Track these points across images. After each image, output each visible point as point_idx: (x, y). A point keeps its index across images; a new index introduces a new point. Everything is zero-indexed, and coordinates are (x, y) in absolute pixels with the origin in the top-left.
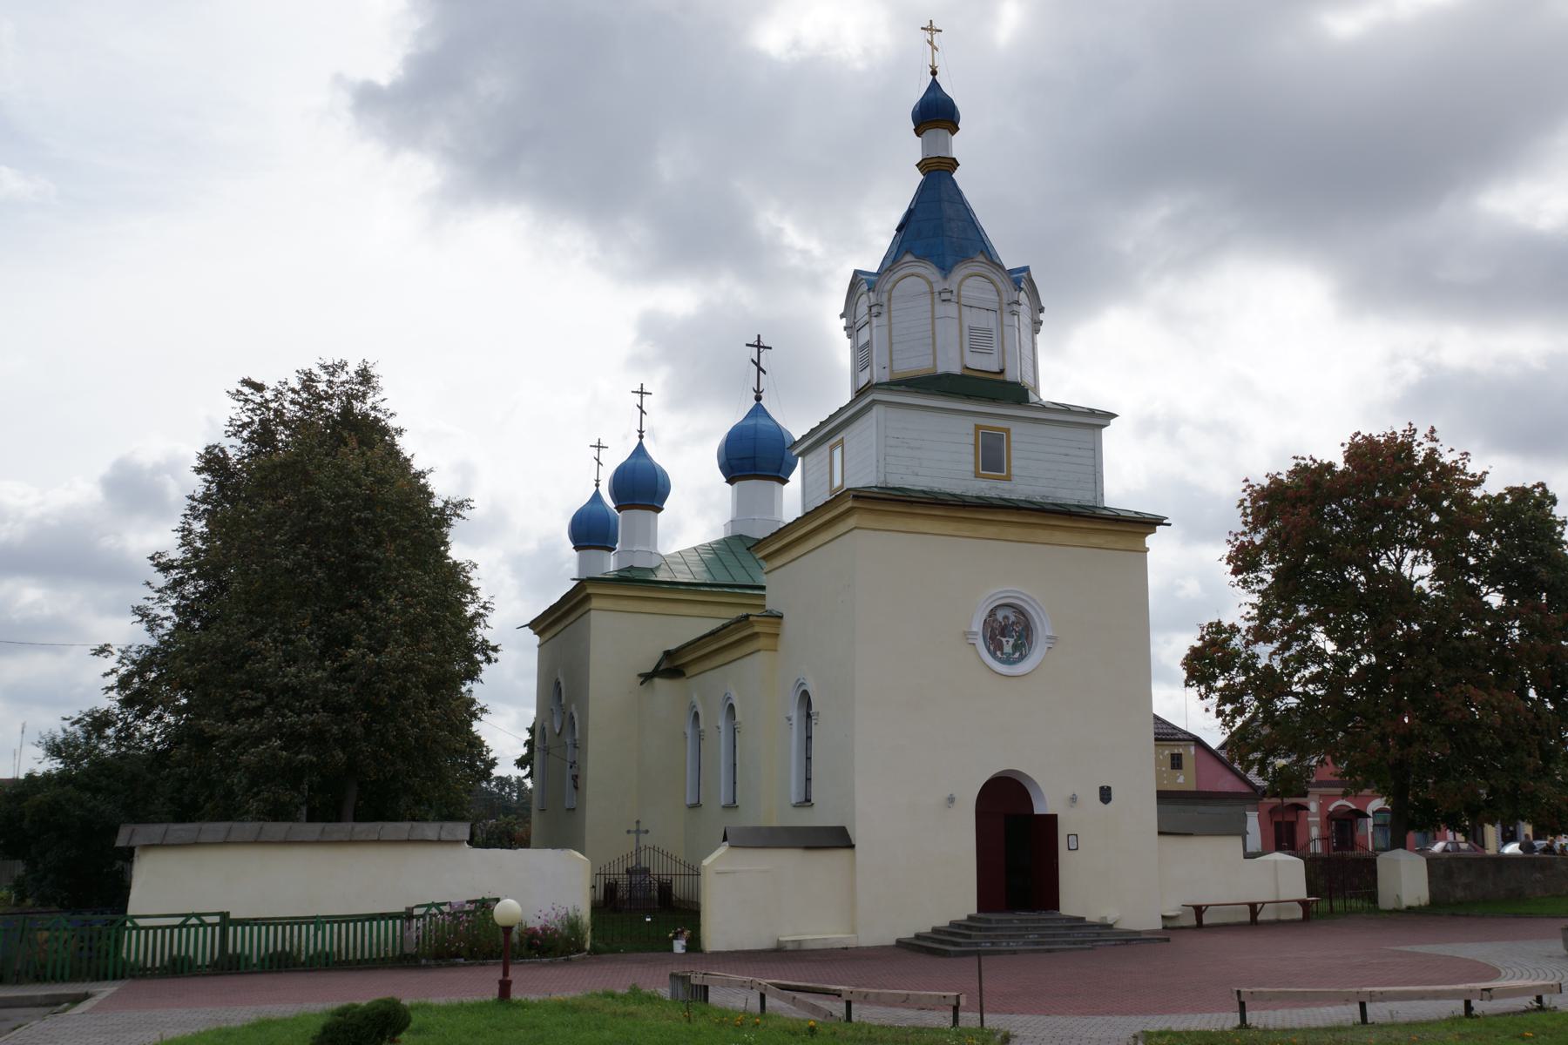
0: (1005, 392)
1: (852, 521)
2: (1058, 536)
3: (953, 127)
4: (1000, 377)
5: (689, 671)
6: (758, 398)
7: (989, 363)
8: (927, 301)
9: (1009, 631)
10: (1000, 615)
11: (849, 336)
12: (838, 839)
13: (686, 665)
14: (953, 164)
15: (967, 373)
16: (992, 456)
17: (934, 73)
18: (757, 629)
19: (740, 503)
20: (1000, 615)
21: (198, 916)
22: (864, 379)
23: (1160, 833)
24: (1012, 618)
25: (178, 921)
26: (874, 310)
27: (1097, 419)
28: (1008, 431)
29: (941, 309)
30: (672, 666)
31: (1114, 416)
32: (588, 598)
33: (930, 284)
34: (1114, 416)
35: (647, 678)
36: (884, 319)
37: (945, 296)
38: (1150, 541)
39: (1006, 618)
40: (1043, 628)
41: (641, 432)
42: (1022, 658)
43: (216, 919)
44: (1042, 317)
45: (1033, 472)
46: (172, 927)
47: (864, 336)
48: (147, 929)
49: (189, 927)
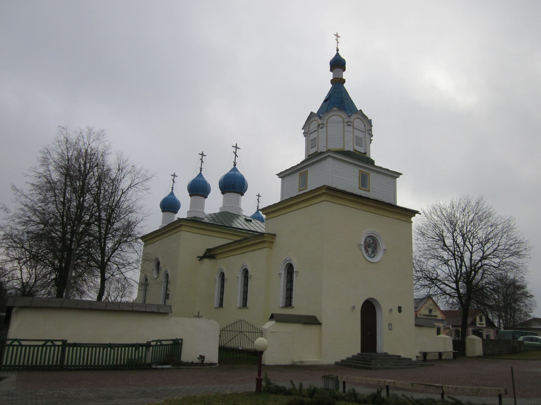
0: (363, 159)
1: (323, 198)
2: (386, 214)
3: (344, 70)
4: (364, 155)
5: (218, 257)
6: (235, 165)
7: (361, 150)
8: (341, 125)
9: (372, 245)
10: (368, 240)
11: (305, 136)
12: (312, 321)
13: (217, 254)
14: (344, 81)
15: (355, 152)
16: (364, 181)
17: (338, 50)
18: (266, 239)
19: (225, 201)
20: (368, 240)
21: (52, 341)
22: (313, 151)
23: (416, 325)
24: (371, 241)
25: (41, 343)
26: (321, 126)
27: (395, 175)
28: (369, 174)
29: (347, 128)
30: (210, 254)
31: (401, 174)
32: (181, 226)
33: (343, 119)
34: (401, 174)
35: (201, 258)
36: (324, 129)
37: (349, 123)
38: (413, 219)
39: (369, 241)
40: (382, 246)
41: (173, 188)
42: (374, 256)
43: (60, 343)
44: (372, 138)
45: (376, 191)
46: (38, 346)
47: (313, 136)
48: (26, 346)
49: (47, 346)
